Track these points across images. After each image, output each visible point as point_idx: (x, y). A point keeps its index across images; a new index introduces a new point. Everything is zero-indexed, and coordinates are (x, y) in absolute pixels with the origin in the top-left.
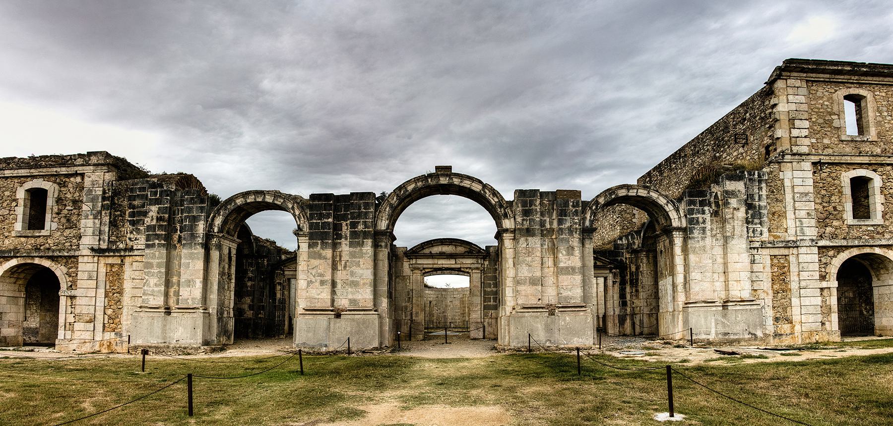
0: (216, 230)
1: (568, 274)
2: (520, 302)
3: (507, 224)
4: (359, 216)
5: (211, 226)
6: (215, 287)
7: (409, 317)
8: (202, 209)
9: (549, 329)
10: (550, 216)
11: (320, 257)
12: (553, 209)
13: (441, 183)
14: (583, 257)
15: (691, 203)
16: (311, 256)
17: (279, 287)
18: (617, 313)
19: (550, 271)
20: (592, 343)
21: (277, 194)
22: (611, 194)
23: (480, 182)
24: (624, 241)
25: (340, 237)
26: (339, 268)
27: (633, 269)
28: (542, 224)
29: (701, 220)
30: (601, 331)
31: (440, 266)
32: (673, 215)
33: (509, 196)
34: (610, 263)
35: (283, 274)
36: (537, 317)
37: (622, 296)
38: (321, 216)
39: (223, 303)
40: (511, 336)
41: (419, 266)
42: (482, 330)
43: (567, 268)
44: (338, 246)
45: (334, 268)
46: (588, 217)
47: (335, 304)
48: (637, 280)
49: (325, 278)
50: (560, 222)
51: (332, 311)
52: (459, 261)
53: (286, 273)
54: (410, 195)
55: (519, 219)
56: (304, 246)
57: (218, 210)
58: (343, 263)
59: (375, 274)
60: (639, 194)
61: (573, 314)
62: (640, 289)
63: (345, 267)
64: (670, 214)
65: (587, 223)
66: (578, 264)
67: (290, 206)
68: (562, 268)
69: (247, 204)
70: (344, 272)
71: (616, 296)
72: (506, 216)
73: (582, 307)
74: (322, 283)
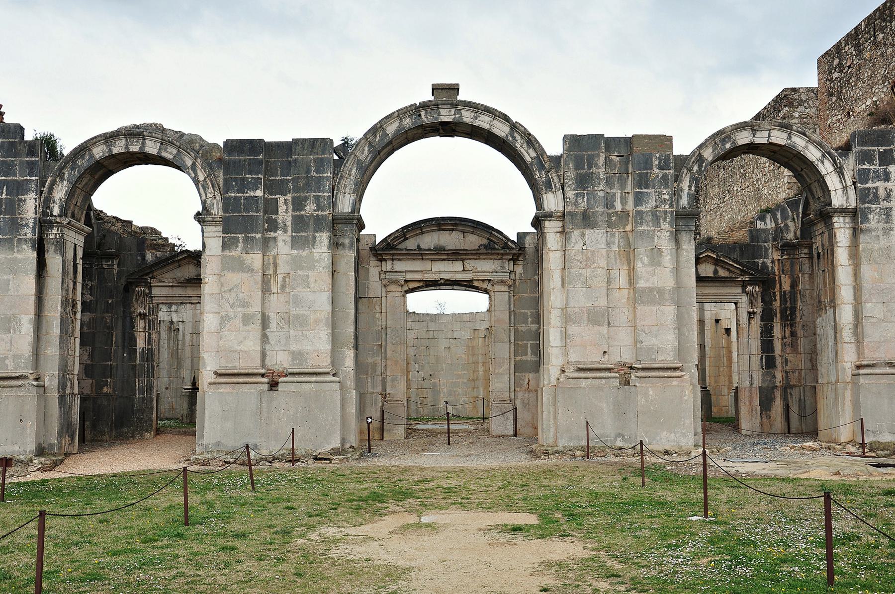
0: (56, 211)
1: (652, 302)
2: (573, 358)
3: (553, 202)
4: (307, 187)
5: (46, 203)
6: (56, 331)
7: (379, 389)
8: (31, 166)
9: (620, 413)
10: (623, 187)
11: (241, 266)
12: (627, 172)
13: (443, 116)
14: (677, 269)
15: (865, 157)
16: (228, 265)
17: (140, 324)
18: (757, 383)
19: (622, 296)
20: (691, 442)
21: (157, 131)
22: (723, 141)
23: (506, 118)
24: (770, 224)
25: (273, 226)
26: (274, 290)
27: (786, 287)
28: (609, 202)
29: (882, 193)
30: (716, 420)
31: (435, 277)
32: (833, 182)
33: (553, 147)
34: (743, 272)
35: (150, 296)
36: (600, 389)
37: (767, 345)
38: (243, 186)
39: (66, 366)
40: (559, 425)
41: (400, 277)
42: (511, 415)
43: (651, 290)
44: (271, 244)
45: (266, 289)
46: (686, 189)
47: (268, 362)
48: (793, 309)
49: (251, 310)
50: (639, 199)
51: (263, 375)
52: (470, 265)
53: (155, 292)
54: (390, 142)
55: (571, 194)
56: (215, 245)
57: (61, 169)
58: (280, 278)
59: (334, 302)
60: (774, 140)
61: (659, 383)
62: (800, 332)
63: (283, 287)
64: (828, 180)
65: (685, 201)
66: (668, 282)
67: (189, 163)
68: (643, 290)
69: (112, 156)
70: (282, 298)
71: (756, 345)
72: (549, 186)
73: (675, 369)
74: (247, 319)
